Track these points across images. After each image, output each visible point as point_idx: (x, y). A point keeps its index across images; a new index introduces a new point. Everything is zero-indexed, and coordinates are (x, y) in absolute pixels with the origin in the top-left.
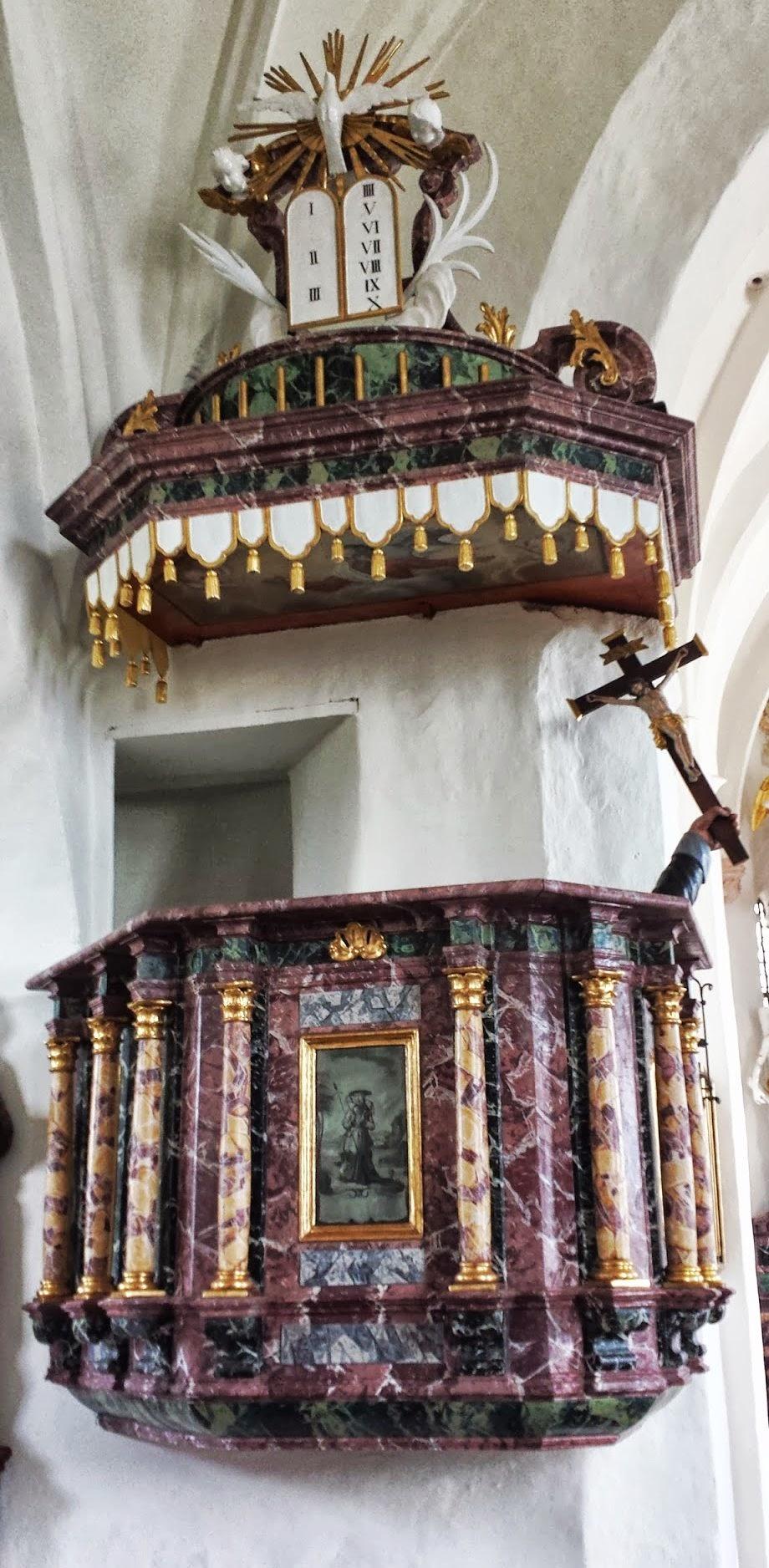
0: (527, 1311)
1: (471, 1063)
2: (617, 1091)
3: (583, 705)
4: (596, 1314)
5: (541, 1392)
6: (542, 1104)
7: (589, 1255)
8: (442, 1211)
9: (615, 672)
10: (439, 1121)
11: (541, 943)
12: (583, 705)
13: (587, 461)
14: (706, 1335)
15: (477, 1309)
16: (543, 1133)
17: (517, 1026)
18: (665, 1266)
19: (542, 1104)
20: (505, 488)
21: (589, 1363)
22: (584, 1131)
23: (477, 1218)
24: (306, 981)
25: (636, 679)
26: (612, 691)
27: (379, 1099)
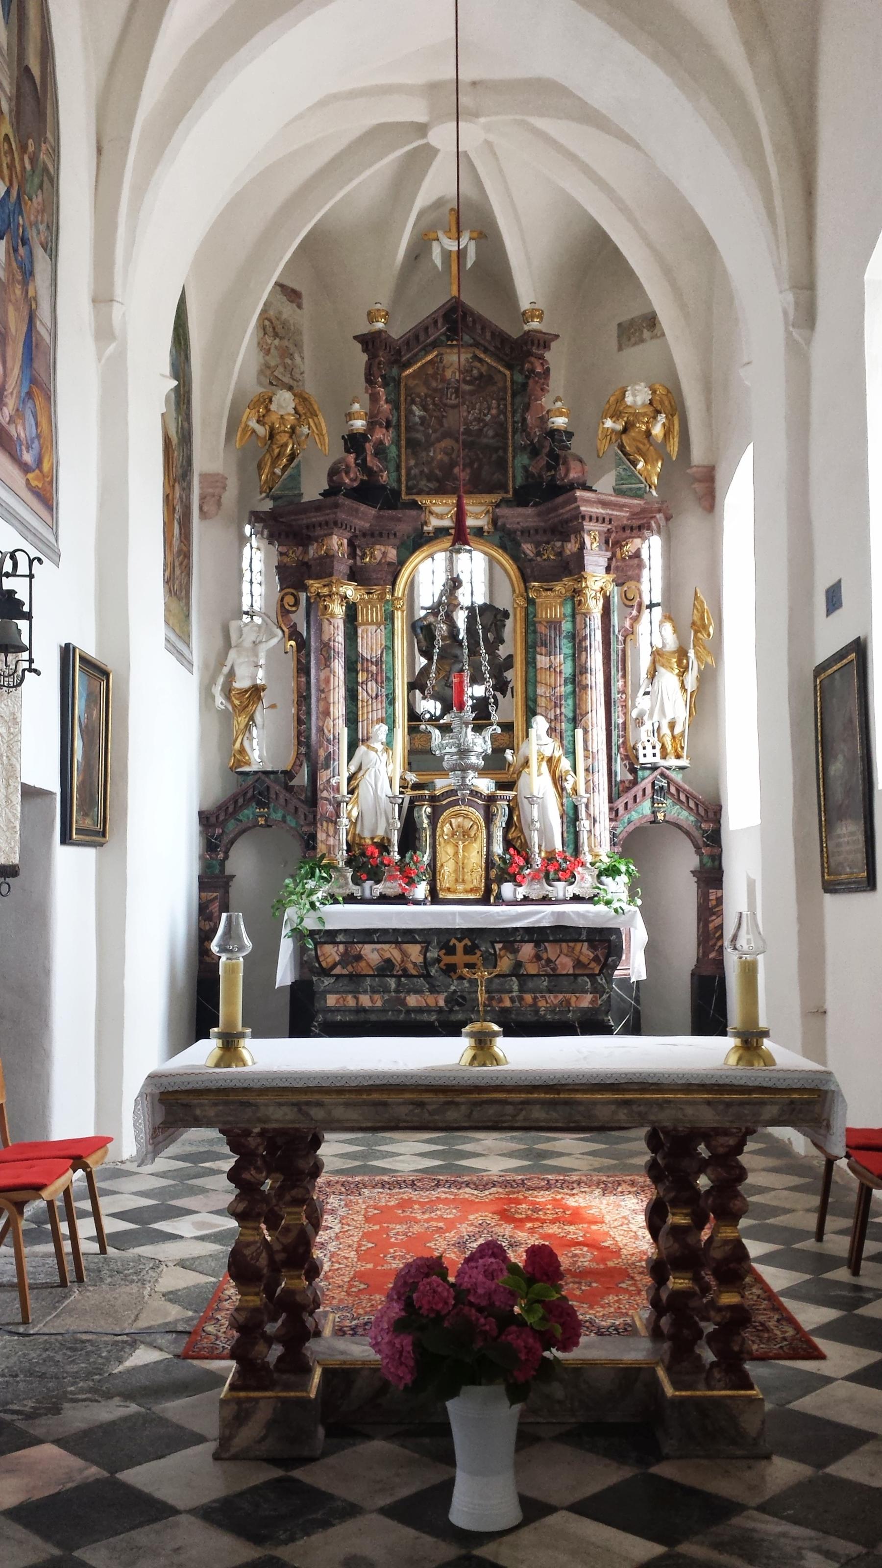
5: (312, 892)
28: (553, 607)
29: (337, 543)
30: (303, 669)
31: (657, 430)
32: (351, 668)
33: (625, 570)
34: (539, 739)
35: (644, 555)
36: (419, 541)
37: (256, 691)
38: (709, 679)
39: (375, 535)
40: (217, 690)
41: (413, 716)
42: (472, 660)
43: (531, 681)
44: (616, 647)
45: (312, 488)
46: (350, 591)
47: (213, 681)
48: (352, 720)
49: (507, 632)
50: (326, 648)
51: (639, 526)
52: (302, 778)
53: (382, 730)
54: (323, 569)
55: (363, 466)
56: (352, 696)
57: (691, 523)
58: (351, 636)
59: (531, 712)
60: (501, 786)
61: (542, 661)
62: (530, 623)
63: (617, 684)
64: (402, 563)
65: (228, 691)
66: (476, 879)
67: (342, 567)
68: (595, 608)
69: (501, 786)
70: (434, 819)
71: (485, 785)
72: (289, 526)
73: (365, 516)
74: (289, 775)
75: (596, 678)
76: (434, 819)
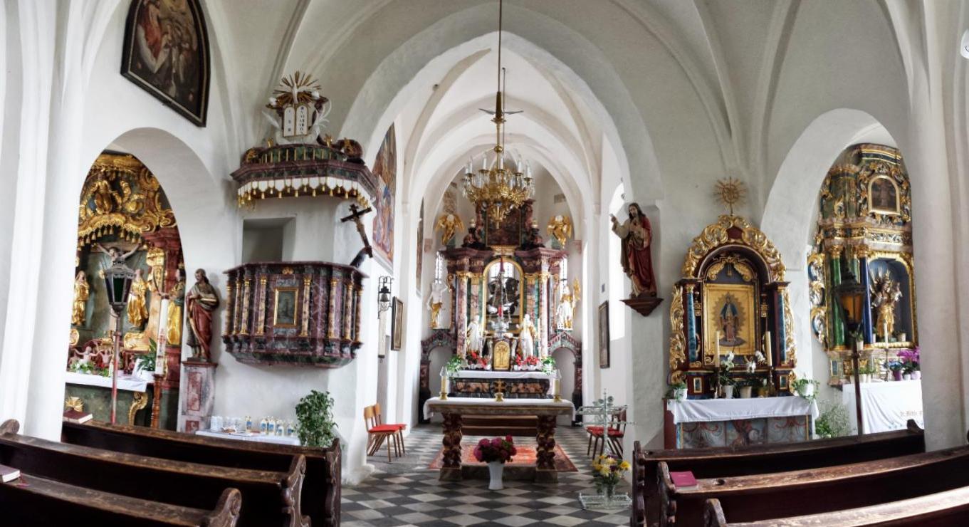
0: (313, 341)
3: (344, 220)
4: (327, 343)
5: (315, 355)
7: (327, 332)
9: (351, 213)
10: (300, 306)
12: (344, 220)
13: (342, 174)
15: (304, 339)
17: (317, 289)
20: (323, 180)
22: (328, 309)
23: (305, 324)
26: (350, 218)
28: (532, 281)
30: (454, 298)
31: (565, 229)
32: (469, 298)
33: (555, 270)
34: (526, 321)
35: (561, 266)
36: (491, 259)
37: (439, 305)
38: (579, 304)
39: (477, 258)
40: (428, 304)
41: (488, 313)
42: (510, 298)
43: (525, 303)
44: (551, 294)
45: (459, 244)
46: (469, 275)
47: (426, 301)
48: (469, 314)
49: (518, 287)
50: (461, 292)
51: (559, 257)
52: (453, 332)
53: (478, 318)
54: (461, 268)
56: (469, 306)
57: (575, 256)
59: (525, 312)
61: (529, 297)
62: (525, 285)
63: (551, 305)
64: (485, 266)
66: (506, 363)
67: (467, 268)
68: (544, 281)
71: (510, 335)
72: (451, 254)
73: (475, 252)
74: (449, 330)
75: (544, 303)
76: (493, 345)
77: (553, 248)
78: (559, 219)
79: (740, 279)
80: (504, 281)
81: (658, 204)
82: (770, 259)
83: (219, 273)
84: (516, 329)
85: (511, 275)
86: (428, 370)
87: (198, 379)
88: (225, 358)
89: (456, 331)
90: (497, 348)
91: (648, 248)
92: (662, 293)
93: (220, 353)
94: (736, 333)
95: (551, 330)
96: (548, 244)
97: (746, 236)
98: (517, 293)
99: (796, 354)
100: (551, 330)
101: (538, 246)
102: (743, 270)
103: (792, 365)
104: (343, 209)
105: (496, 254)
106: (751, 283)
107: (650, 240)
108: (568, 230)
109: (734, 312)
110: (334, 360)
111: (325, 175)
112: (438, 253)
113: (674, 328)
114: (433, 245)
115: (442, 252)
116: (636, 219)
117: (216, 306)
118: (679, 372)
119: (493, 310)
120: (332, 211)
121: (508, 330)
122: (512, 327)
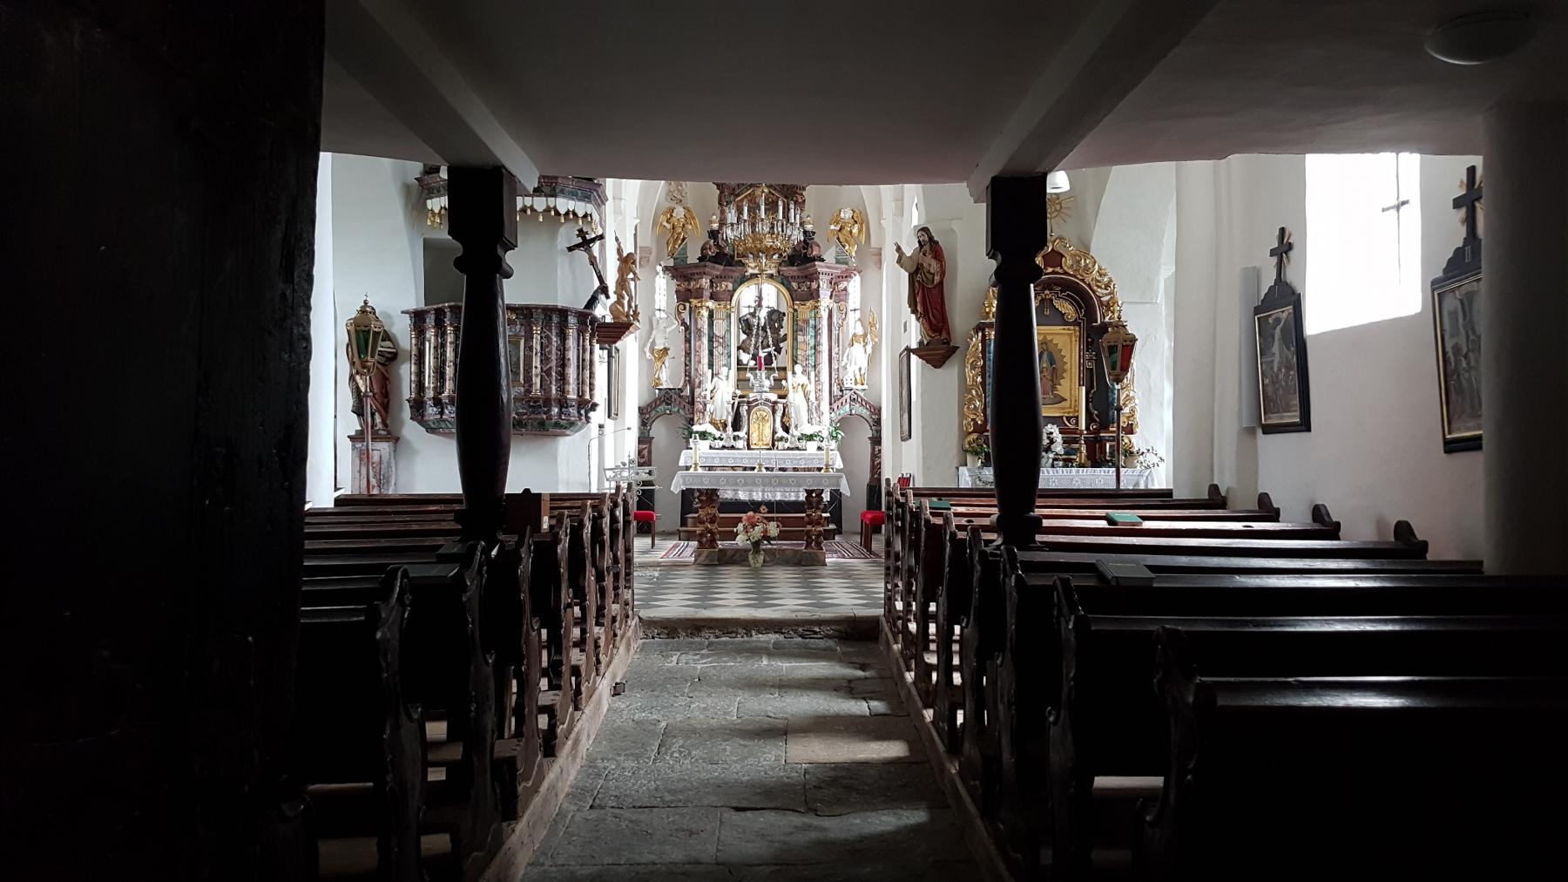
0: (547, 402)
1: (536, 345)
2: (572, 355)
3: (570, 249)
4: (563, 403)
5: (550, 418)
6: (554, 357)
7: (562, 390)
8: (528, 379)
9: (580, 240)
10: (528, 360)
11: (555, 319)
12: (570, 249)
13: (573, 195)
14: (592, 414)
15: (536, 400)
16: (553, 364)
17: (549, 338)
18: (581, 395)
19: (554, 357)
20: (551, 201)
21: (560, 413)
22: (563, 363)
23: (537, 381)
24: (812, 447)
25: (586, 244)
26: (578, 246)
27: (811, 388)
28: (805, 311)
29: (705, 282)
30: (688, 341)
31: (855, 231)
32: (711, 340)
33: (840, 296)
34: (796, 378)
35: (850, 289)
36: (744, 280)
37: (666, 350)
38: (876, 348)
39: (722, 278)
40: (647, 350)
41: (739, 362)
42: (770, 341)
43: (795, 348)
44: (834, 332)
45: (693, 257)
46: (710, 304)
47: (645, 345)
48: (711, 366)
49: (784, 323)
50: (699, 331)
51: (847, 276)
52: (687, 392)
53: (725, 369)
54: (698, 294)
55: (718, 246)
56: (711, 353)
57: (871, 273)
58: (711, 325)
59: (795, 362)
60: (780, 397)
61: (800, 338)
62: (795, 321)
63: (835, 350)
64: (734, 290)
65: (652, 351)
66: (768, 439)
67: (707, 294)
68: (825, 315)
69: (780, 397)
70: (749, 412)
71: (773, 397)
72: (680, 272)
73: (719, 269)
74: (681, 390)
75: (824, 348)
76: (749, 412)
77: (838, 262)
78: (846, 214)
79: (1061, 319)
80: (763, 314)
81: (955, 226)
82: (1100, 292)
83: (396, 314)
84: (781, 387)
85: (774, 305)
86: (650, 452)
87: (376, 459)
88: (411, 430)
89: (692, 392)
90: (753, 416)
91: (941, 283)
92: (957, 340)
93: (402, 423)
94: (1053, 388)
95: (835, 388)
96: (830, 256)
97: (1067, 262)
98: (782, 332)
99: (1137, 415)
100: (835, 388)
101: (814, 259)
102: (1067, 308)
103: (1130, 430)
104: (567, 235)
105: (751, 271)
106: (1075, 323)
107: (943, 274)
108: (860, 231)
109: (1052, 361)
110: (572, 424)
111: (554, 196)
112: (659, 268)
113: (969, 382)
114: (652, 258)
115: (666, 269)
116: (927, 247)
117: (392, 358)
118: (975, 436)
119: (745, 358)
120: (553, 235)
121: (772, 389)
122: (778, 385)
